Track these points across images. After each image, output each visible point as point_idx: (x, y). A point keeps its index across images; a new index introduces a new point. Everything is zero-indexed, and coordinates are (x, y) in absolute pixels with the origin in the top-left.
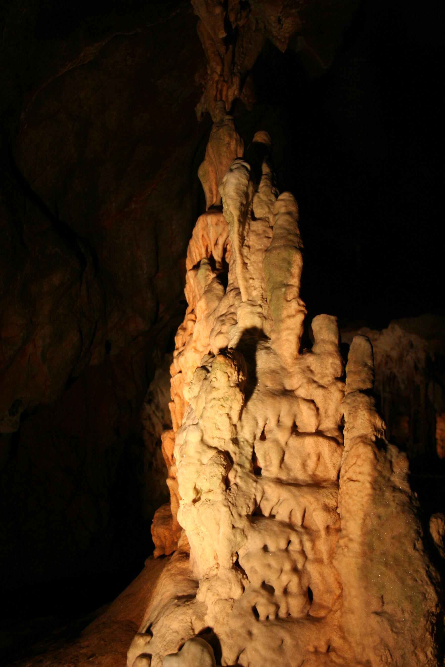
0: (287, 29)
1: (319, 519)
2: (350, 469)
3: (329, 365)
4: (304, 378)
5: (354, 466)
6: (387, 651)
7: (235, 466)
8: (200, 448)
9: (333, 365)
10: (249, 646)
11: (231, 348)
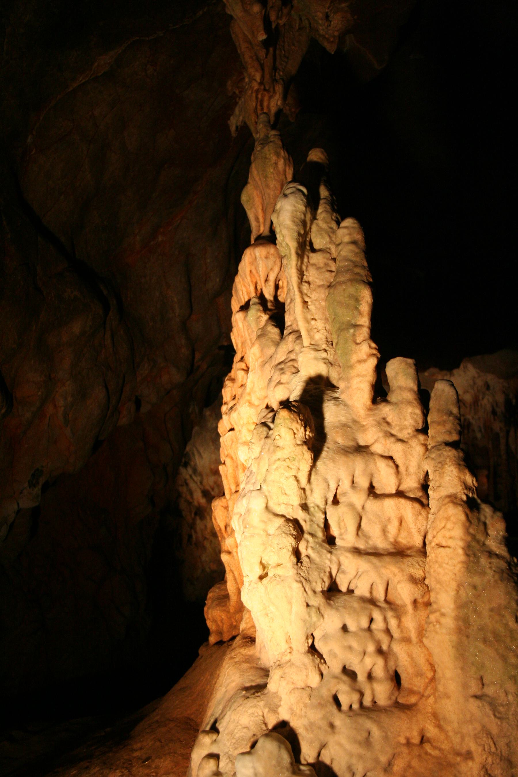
0: (335, 27)
1: (405, 593)
2: (439, 534)
3: (408, 415)
4: (380, 431)
5: (443, 530)
6: (490, 740)
7: (306, 536)
8: (267, 516)
9: (413, 415)
10: (332, 740)
11: (295, 401)
